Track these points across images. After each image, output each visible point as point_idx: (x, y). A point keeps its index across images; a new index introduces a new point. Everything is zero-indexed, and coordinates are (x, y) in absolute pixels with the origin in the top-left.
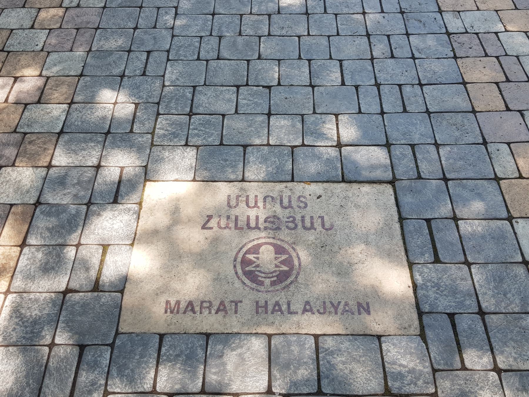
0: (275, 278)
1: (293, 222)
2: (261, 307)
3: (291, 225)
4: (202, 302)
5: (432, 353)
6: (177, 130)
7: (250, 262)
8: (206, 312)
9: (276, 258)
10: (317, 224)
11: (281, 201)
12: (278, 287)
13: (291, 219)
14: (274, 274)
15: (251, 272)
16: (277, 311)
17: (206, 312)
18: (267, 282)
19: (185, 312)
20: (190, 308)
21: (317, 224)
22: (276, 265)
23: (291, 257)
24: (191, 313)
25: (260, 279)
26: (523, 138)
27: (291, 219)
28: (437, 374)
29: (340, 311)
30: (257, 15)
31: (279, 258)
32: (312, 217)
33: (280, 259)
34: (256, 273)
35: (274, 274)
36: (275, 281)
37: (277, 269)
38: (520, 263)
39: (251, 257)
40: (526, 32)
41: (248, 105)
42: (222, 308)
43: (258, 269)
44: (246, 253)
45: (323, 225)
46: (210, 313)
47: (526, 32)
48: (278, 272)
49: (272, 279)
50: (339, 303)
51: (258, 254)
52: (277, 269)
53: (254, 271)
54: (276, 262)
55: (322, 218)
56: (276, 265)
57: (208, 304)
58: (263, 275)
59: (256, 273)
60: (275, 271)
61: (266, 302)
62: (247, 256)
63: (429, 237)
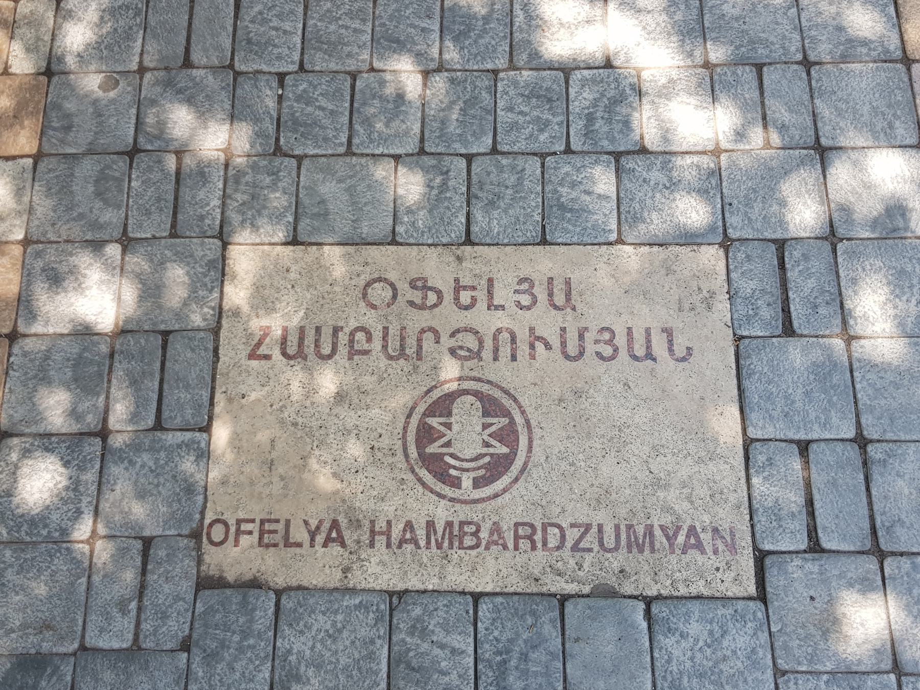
0: (481, 472)
1: (610, 342)
2: (382, 533)
5: (766, 234)
6: (303, 109)
7: (499, 436)
9: (485, 427)
10: (659, 346)
11: (564, 344)
12: (487, 491)
13: (607, 336)
14: (481, 462)
15: (439, 457)
16: (334, 540)
18: (467, 482)
20: (671, 533)
22: (450, 429)
23: (512, 422)
25: (453, 472)
27: (607, 336)
29: (320, 539)
30: (650, 245)
31: (492, 424)
33: (493, 429)
34: (448, 459)
35: (481, 462)
36: (482, 477)
39: (434, 422)
42: (408, 536)
43: (451, 450)
44: (425, 415)
46: (534, 548)
48: (487, 459)
50: (321, 522)
51: (450, 414)
52: (485, 450)
54: (449, 435)
56: (450, 429)
57: (529, 531)
58: (466, 465)
59: (448, 459)
60: (481, 456)
61: (389, 523)
63: (790, 294)
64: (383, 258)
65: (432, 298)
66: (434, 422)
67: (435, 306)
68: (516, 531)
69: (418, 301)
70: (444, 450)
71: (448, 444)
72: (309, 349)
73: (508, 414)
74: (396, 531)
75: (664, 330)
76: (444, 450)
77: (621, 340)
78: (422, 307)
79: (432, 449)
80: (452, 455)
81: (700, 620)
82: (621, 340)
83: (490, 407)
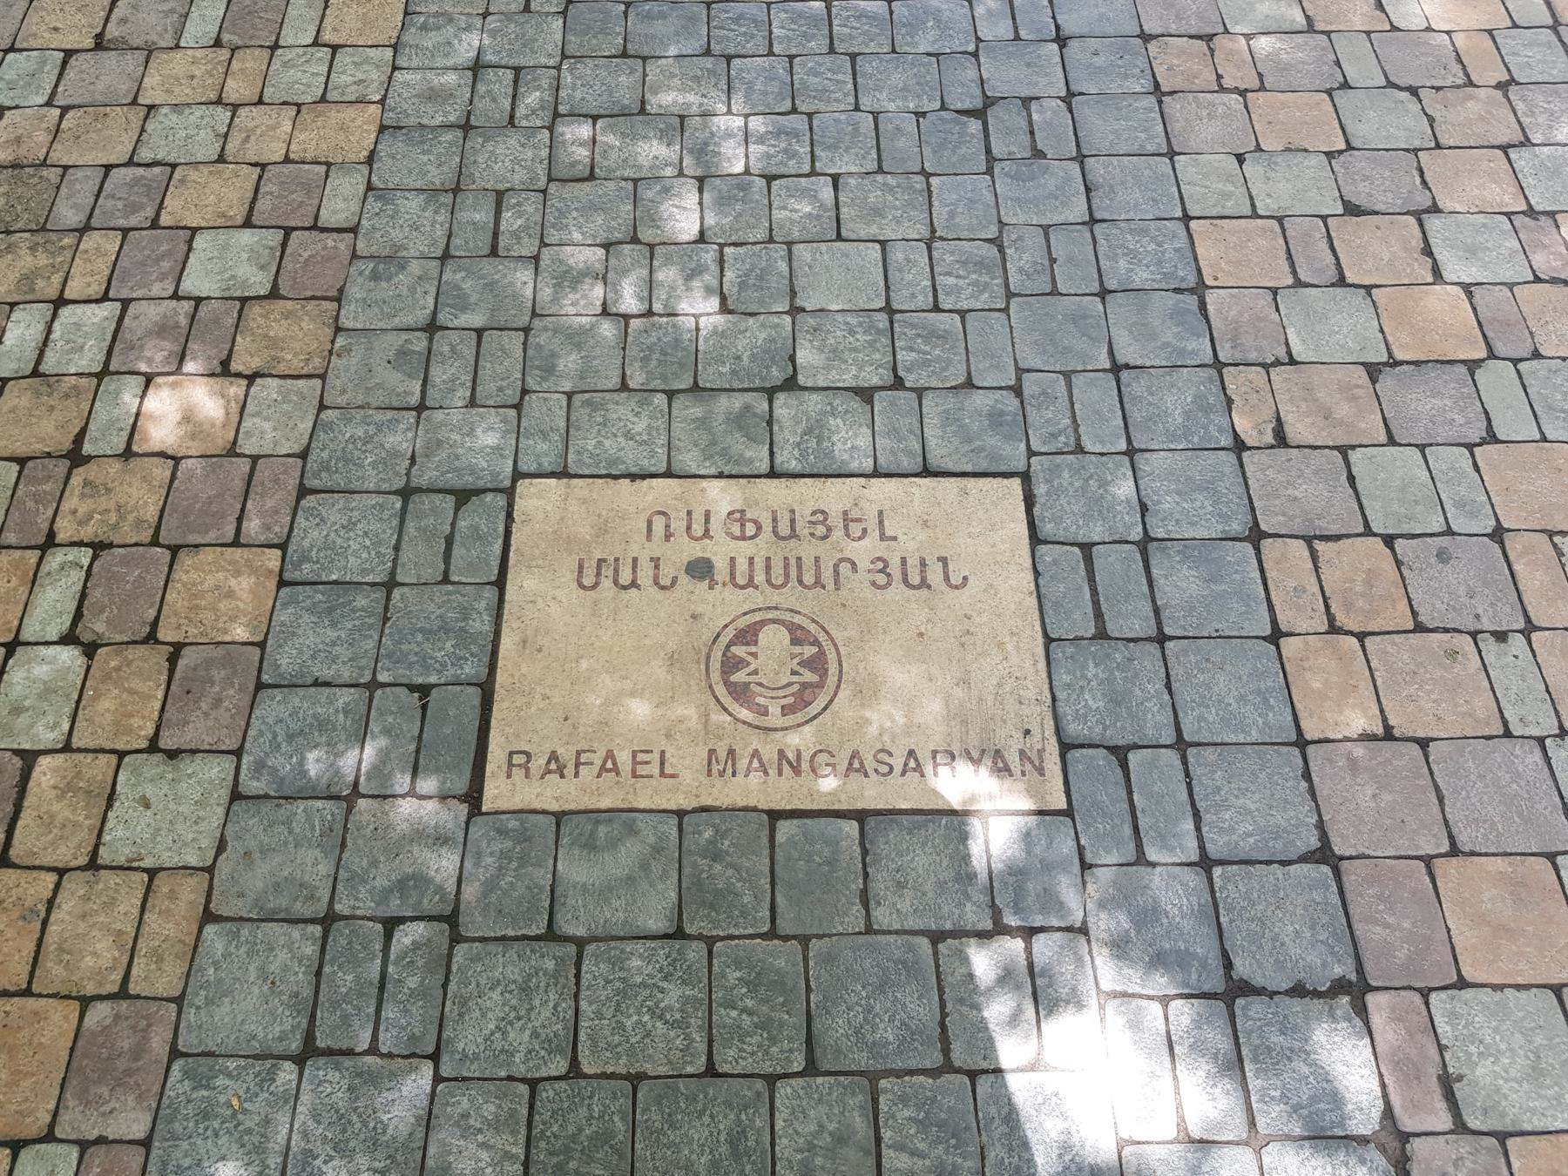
0: (791, 700)
3: (881, 579)
4: (511, 754)
8: (518, 774)
10: (645, 574)
12: (799, 717)
16: (609, 771)
17: (518, 774)
18: (775, 710)
19: (904, 773)
21: (645, 574)
23: (822, 653)
24: (555, 778)
26: (1555, 74)
27: (880, 565)
28: (75, 1006)
32: (923, 563)
33: (747, 670)
37: (795, 678)
38: (62, 291)
39: (739, 651)
40: (1557, 990)
41: (789, 39)
44: (728, 647)
45: (947, 578)
47: (1557, 990)
48: (796, 687)
49: (785, 701)
53: (747, 684)
55: (944, 560)
60: (789, 684)
62: (733, 649)
64: (776, 493)
65: (750, 529)
66: (739, 651)
67: (752, 538)
68: (634, 757)
69: (737, 533)
70: (751, 679)
71: (755, 672)
72: (760, 578)
73: (816, 642)
74: (898, 764)
75: (652, 559)
76: (751, 679)
77: (895, 568)
78: (743, 538)
79: (739, 677)
80: (760, 684)
81: (685, 1001)
82: (895, 568)
83: (798, 636)
